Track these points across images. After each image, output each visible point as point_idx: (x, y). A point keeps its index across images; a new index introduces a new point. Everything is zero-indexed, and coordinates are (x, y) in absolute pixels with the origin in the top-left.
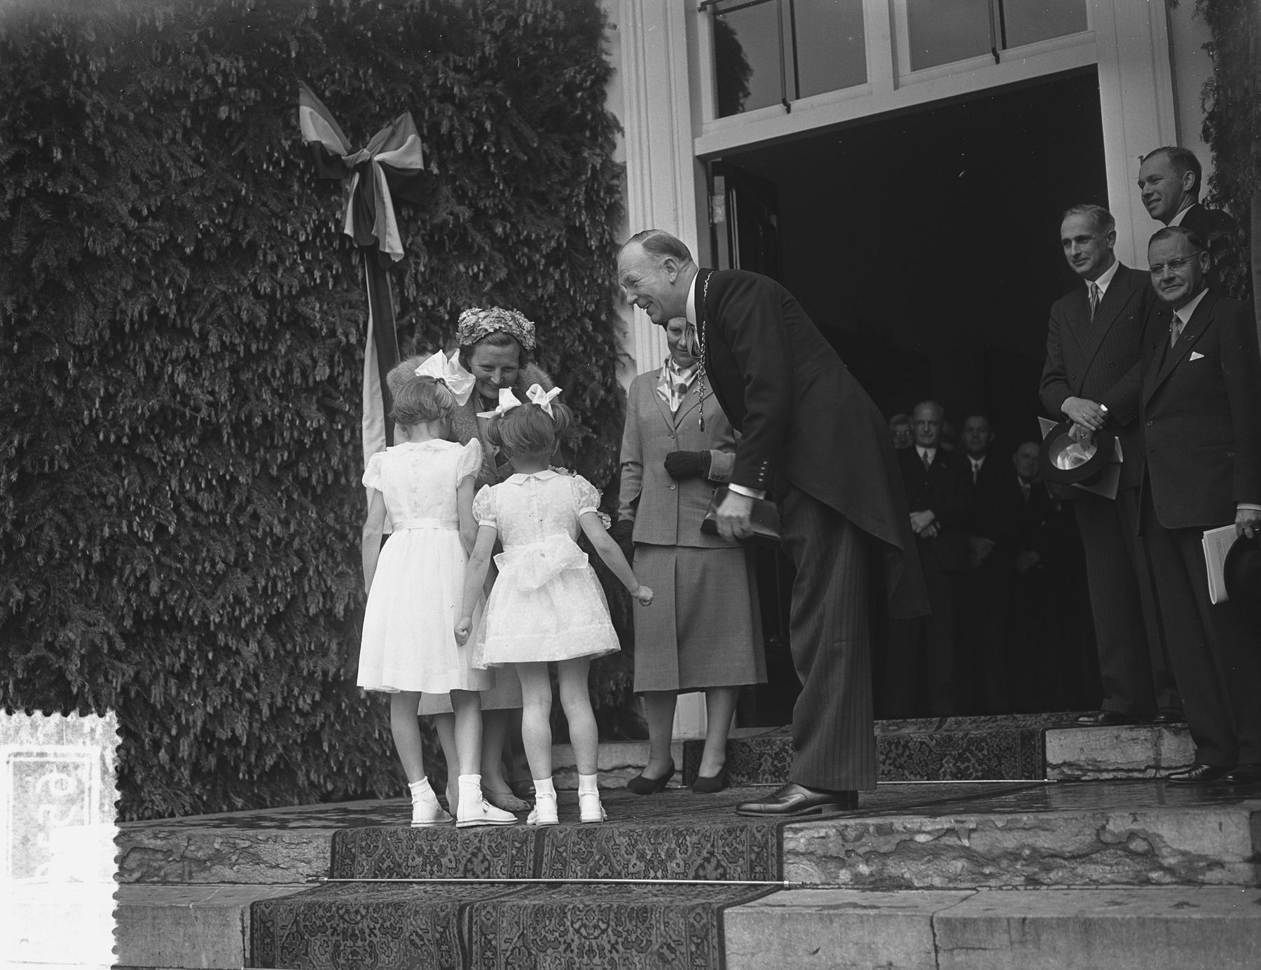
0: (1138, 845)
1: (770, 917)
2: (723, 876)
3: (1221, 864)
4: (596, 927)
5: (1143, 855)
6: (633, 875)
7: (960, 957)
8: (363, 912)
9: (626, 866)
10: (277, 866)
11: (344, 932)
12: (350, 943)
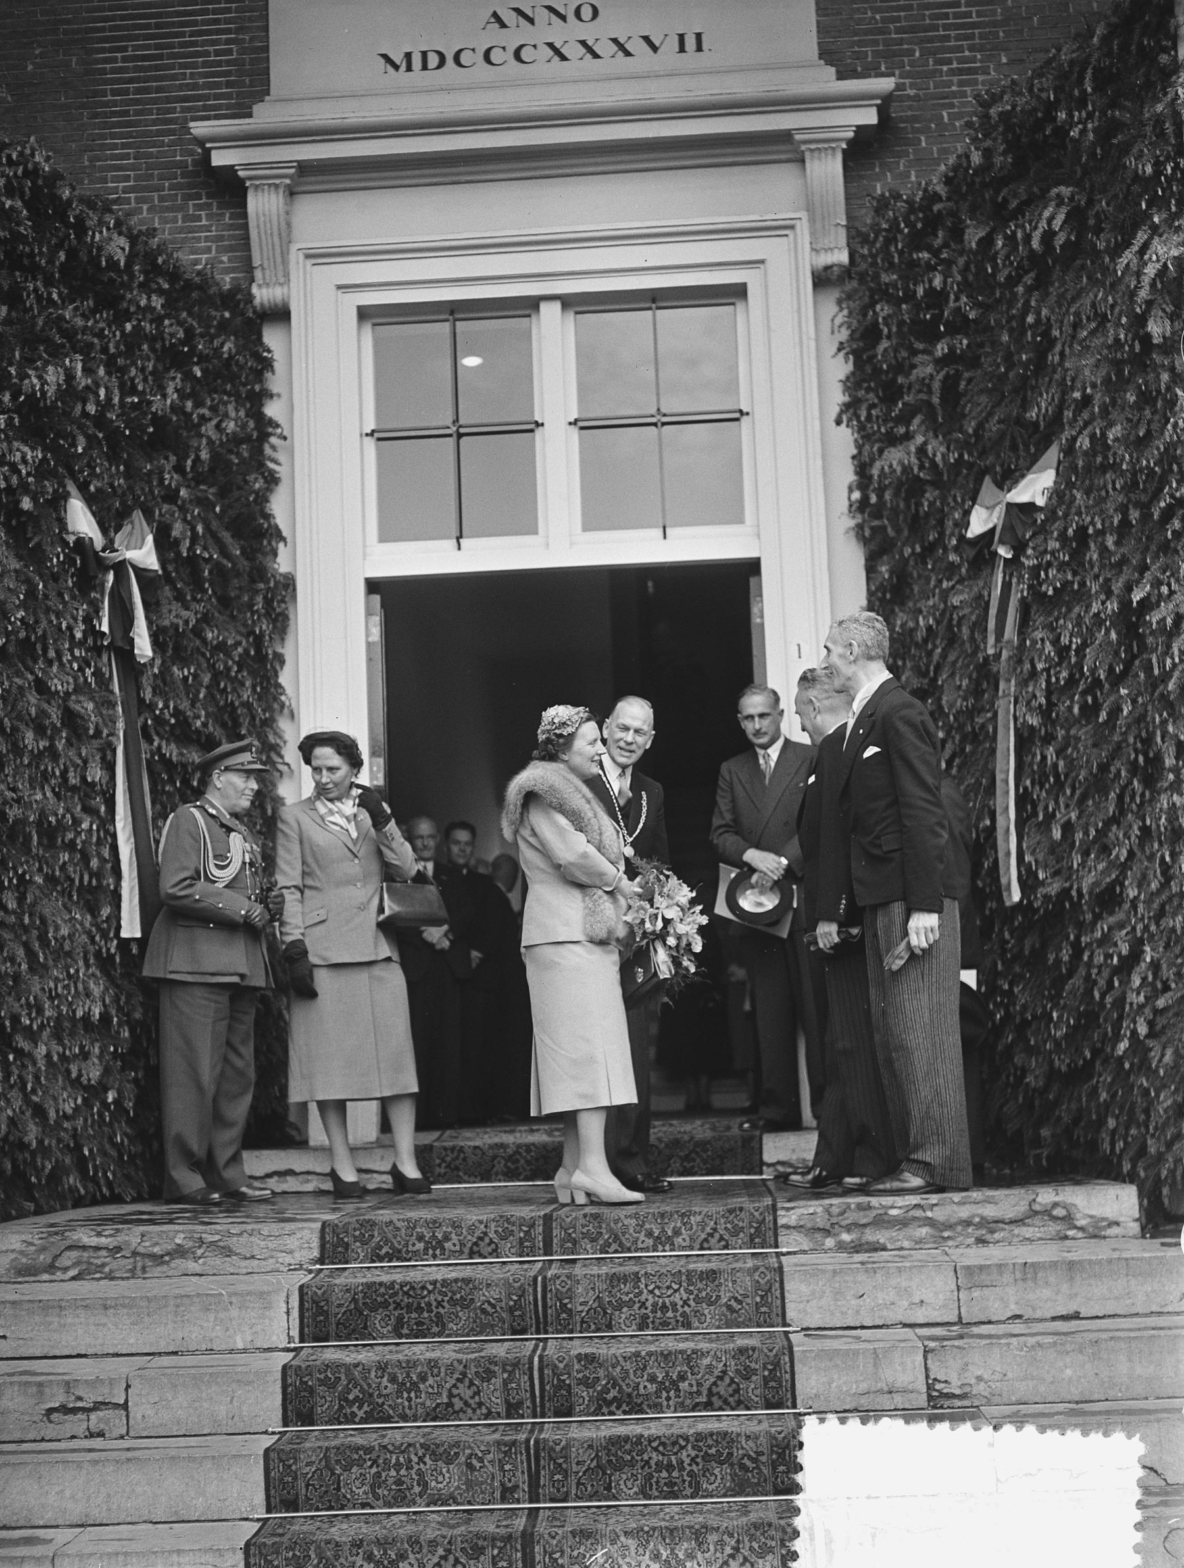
0: (1059, 1212)
1: (823, 1271)
2: (726, 1247)
3: (1117, 1224)
4: (668, 1288)
5: (1062, 1219)
6: (642, 1250)
7: (976, 1293)
8: (430, 1287)
9: (635, 1242)
10: (253, 1257)
11: (409, 1306)
12: (414, 1315)
